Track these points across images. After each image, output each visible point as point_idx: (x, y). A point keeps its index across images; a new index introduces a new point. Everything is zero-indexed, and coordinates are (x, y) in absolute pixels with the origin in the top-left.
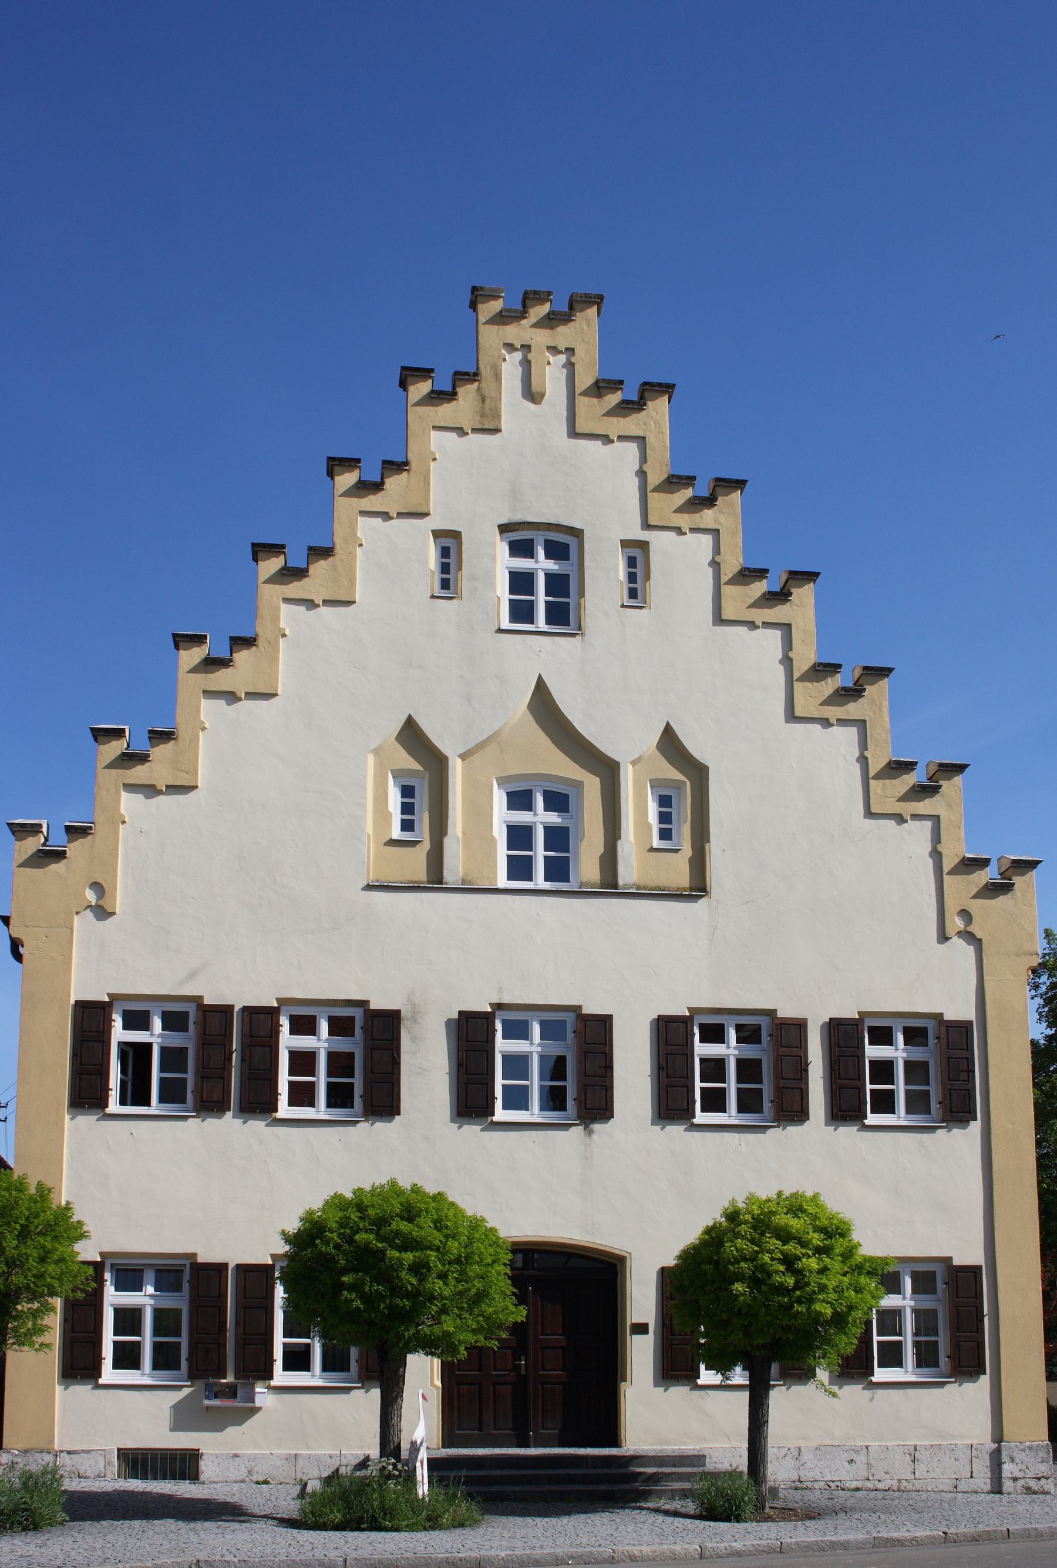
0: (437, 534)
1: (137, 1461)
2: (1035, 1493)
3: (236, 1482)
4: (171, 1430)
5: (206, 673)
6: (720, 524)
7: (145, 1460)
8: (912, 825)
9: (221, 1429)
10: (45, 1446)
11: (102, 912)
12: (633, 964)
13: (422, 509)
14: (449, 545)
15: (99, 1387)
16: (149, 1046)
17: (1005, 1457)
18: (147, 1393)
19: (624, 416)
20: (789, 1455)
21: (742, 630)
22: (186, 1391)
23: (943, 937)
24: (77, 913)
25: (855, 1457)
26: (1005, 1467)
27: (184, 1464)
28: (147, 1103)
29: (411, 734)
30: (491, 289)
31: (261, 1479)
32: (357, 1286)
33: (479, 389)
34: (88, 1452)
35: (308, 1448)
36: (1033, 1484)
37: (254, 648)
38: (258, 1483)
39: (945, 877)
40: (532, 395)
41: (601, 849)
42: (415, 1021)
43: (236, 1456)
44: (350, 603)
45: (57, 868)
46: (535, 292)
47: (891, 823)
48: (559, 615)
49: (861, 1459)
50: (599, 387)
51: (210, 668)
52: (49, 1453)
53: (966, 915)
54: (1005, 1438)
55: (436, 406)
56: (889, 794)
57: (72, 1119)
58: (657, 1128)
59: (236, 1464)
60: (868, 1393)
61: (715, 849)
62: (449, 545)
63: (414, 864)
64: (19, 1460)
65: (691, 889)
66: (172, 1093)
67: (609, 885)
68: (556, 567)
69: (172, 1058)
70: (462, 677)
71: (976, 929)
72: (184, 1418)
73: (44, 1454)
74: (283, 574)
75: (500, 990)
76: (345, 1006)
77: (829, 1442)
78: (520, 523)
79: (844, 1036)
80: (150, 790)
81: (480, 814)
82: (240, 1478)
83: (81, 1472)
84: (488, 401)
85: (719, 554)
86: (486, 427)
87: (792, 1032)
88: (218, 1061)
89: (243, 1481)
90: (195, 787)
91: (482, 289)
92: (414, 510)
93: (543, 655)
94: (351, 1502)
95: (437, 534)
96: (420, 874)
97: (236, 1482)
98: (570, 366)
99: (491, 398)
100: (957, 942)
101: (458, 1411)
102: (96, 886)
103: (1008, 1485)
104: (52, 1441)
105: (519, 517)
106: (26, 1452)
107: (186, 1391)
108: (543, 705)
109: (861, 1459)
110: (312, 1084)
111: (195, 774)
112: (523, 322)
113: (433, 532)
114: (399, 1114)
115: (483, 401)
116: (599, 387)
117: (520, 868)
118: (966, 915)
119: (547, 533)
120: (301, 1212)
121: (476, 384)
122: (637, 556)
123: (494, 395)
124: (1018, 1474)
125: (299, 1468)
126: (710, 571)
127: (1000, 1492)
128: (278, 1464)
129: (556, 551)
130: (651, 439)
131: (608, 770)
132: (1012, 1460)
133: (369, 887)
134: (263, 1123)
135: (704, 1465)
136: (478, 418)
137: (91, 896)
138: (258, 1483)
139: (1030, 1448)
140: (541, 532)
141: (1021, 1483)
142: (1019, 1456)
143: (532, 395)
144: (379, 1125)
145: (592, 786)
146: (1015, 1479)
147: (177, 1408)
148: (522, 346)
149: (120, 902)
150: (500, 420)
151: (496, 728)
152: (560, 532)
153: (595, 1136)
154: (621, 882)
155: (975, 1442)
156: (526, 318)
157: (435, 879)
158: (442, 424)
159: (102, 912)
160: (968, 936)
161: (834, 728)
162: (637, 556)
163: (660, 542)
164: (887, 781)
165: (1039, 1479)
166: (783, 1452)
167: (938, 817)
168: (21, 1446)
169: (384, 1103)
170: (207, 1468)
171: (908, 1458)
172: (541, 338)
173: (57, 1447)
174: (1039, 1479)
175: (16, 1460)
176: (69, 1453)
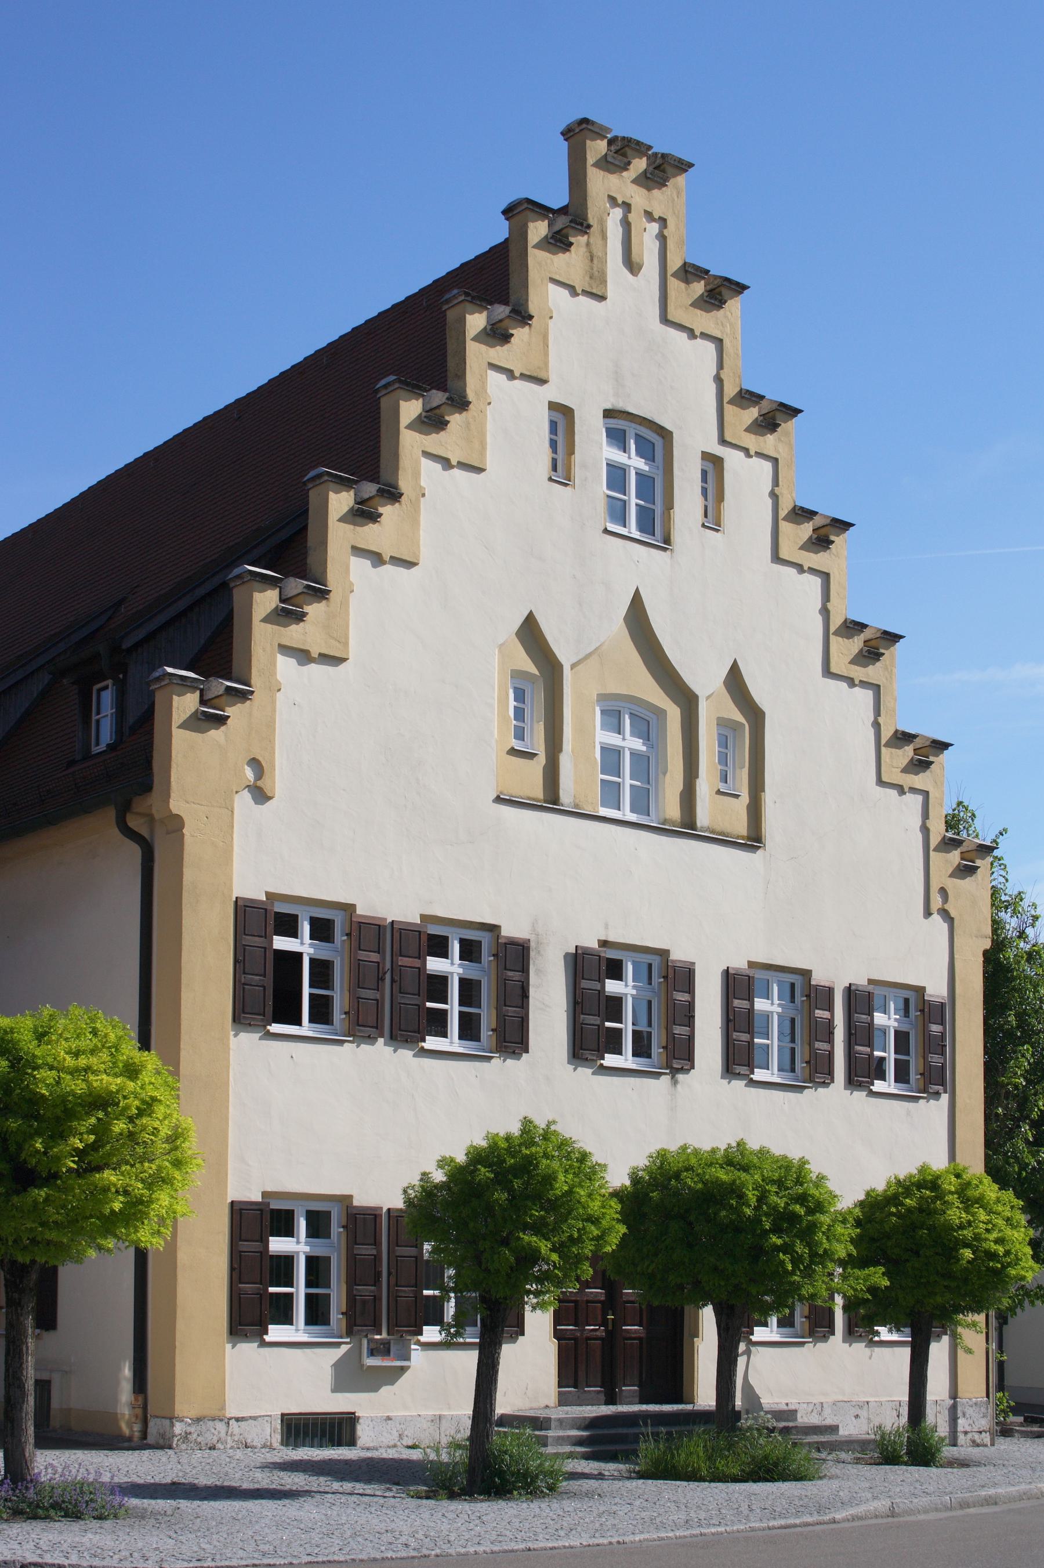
0: (553, 406)
1: (299, 1428)
2: (978, 1445)
3: (389, 1447)
4: (333, 1391)
5: (355, 524)
6: (778, 452)
7: (315, 1424)
8: (909, 797)
9: (375, 1389)
10: (217, 1413)
11: (261, 795)
12: (705, 912)
13: (542, 375)
14: (562, 416)
15: (264, 1344)
16: (299, 956)
17: (960, 1414)
18: (308, 1351)
19: (708, 311)
20: (815, 1411)
21: (792, 571)
22: (344, 1348)
23: (928, 913)
24: (237, 792)
25: (859, 1412)
26: (960, 1421)
27: (338, 1429)
28: (298, 1022)
29: (530, 633)
30: (601, 127)
31: (410, 1444)
32: (481, 1236)
33: (588, 244)
34: (254, 1418)
35: (450, 1409)
36: (977, 1437)
37: (397, 504)
38: (409, 1447)
39: (932, 853)
40: (632, 265)
41: (680, 786)
42: (539, 952)
43: (389, 1418)
44: (479, 470)
45: (216, 734)
46: (638, 143)
47: (894, 793)
48: (646, 522)
49: (863, 1414)
50: (686, 271)
51: (359, 520)
52: (221, 1420)
53: (943, 892)
54: (960, 1394)
55: (554, 254)
56: (895, 765)
57: (236, 1035)
58: (725, 1082)
59: (388, 1427)
60: (868, 1351)
61: (769, 797)
62: (562, 416)
63: (529, 778)
64: (192, 1429)
65: (749, 838)
66: (321, 1013)
67: (687, 827)
68: (647, 468)
69: (322, 971)
70: (574, 577)
71: (949, 907)
72: (347, 1377)
73: (217, 1422)
74: (423, 422)
75: (606, 926)
76: (478, 929)
77: (841, 1398)
78: (621, 412)
79: (860, 1001)
80: (303, 656)
81: (584, 732)
82: (392, 1443)
83: (249, 1441)
84: (595, 261)
85: (777, 486)
86: (594, 291)
87: (515, 956)
88: (383, 980)
89: (395, 1446)
90: (344, 660)
91: (593, 123)
92: (535, 374)
93: (633, 566)
94: (487, 1466)
95: (553, 406)
96: (536, 790)
97: (389, 1447)
98: (662, 238)
99: (598, 257)
100: (936, 918)
101: (573, 1368)
102: (255, 764)
103: (961, 1439)
104: (223, 1408)
105: (621, 405)
106: (198, 1420)
107: (344, 1348)
108: (637, 618)
109: (863, 1414)
110: (444, 1012)
111: (346, 644)
112: (625, 174)
113: (550, 403)
114: (527, 1052)
115: (592, 260)
116: (686, 271)
117: (611, 794)
118: (943, 892)
119: (638, 427)
120: (653, 1148)
121: (586, 237)
122: (713, 464)
123: (600, 254)
124: (968, 1429)
125: (442, 1430)
126: (769, 502)
127: (955, 1445)
128: (425, 1426)
129: (646, 450)
130: (727, 343)
131: (687, 700)
132: (964, 1415)
133: (499, 800)
134: (410, 1053)
135: (796, 1420)
136: (587, 278)
137: (249, 774)
138: (409, 1447)
139: (976, 1404)
140: (633, 425)
141: (969, 1436)
142: (970, 1411)
143: (632, 265)
144: (510, 1062)
145: (674, 714)
146: (966, 1433)
147: (338, 1366)
148: (623, 202)
149: (280, 782)
150: (606, 286)
151: (602, 640)
152: (650, 428)
153: (679, 1086)
154: (699, 824)
155: (938, 1398)
156: (627, 169)
157: (551, 801)
158: (557, 277)
159: (261, 795)
160: (945, 914)
161: (857, 689)
162: (713, 464)
163: (733, 459)
164: (894, 750)
165: (981, 1432)
166: (811, 1406)
167: (927, 792)
168: (194, 1413)
169: (513, 1039)
170: (365, 1434)
171: (895, 1413)
172: (638, 197)
173: (228, 1415)
174: (981, 1432)
175: (189, 1429)
176: (238, 1420)
